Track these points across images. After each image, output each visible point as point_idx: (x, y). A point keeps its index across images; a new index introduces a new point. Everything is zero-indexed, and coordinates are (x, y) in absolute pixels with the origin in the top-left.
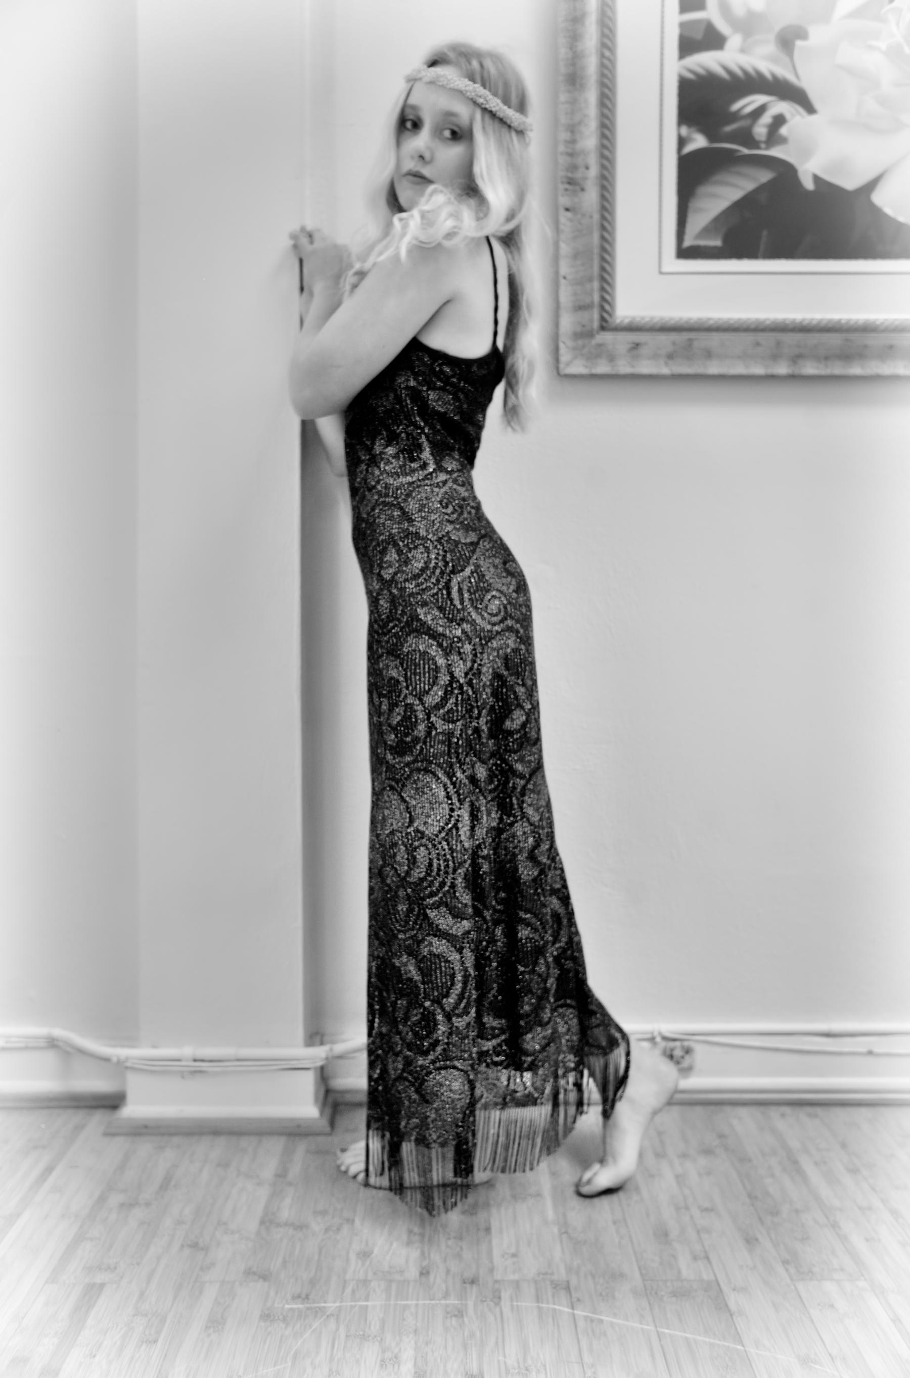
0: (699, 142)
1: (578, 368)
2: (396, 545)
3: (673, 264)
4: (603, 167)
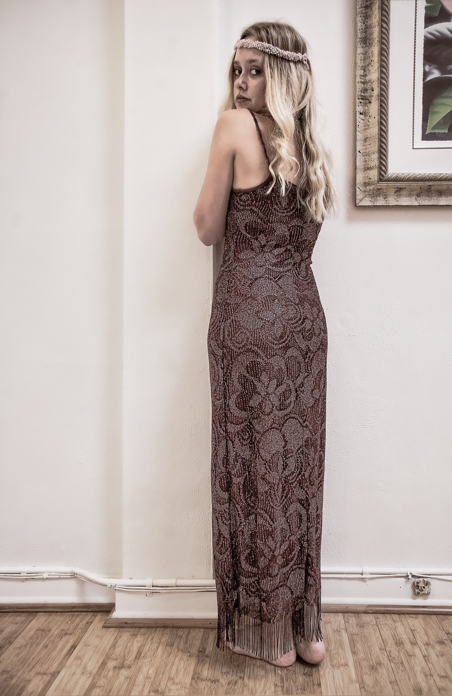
0: (436, 74)
1: (367, 202)
3: (420, 143)
4: (381, 89)
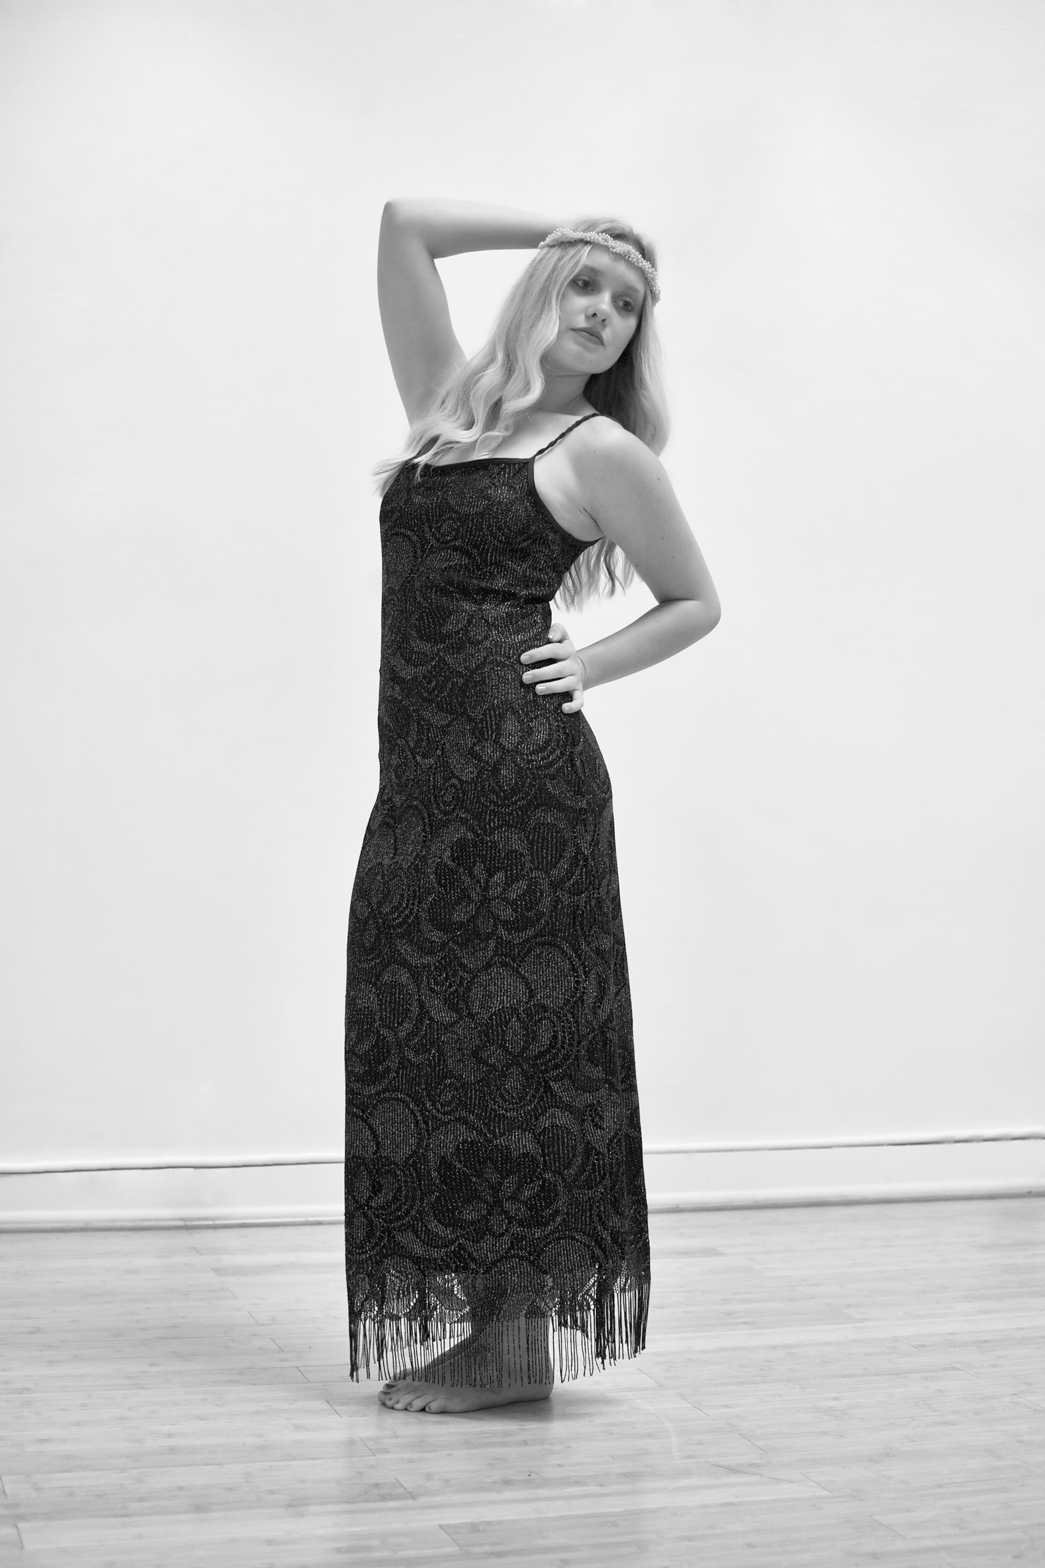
2: (515, 712)
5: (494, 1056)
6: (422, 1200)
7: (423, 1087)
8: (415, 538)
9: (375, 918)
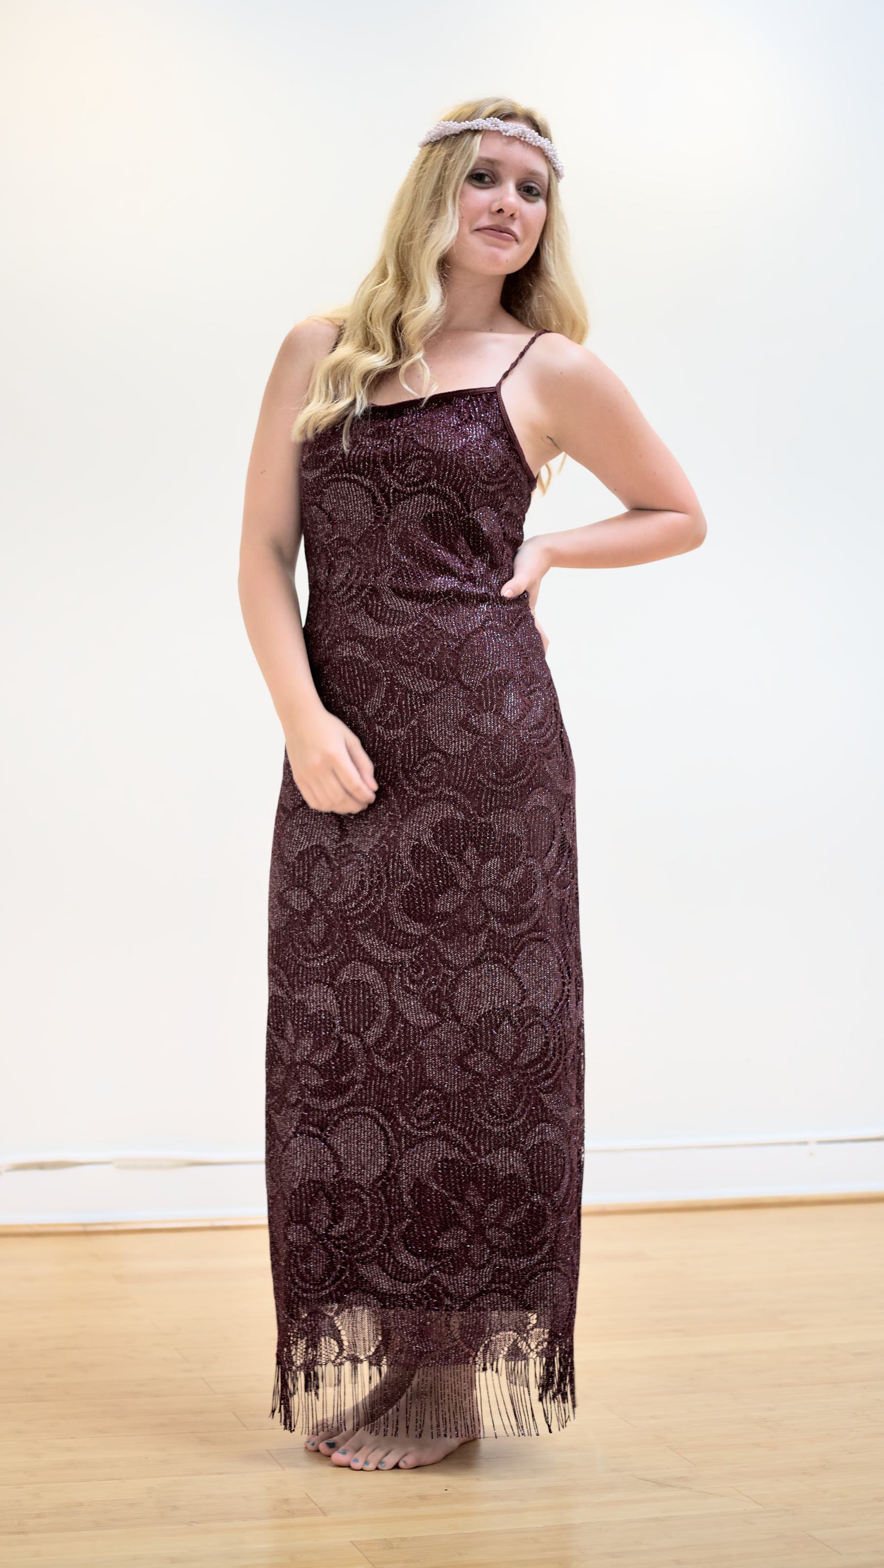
5: (481, 1063)
6: (390, 1228)
7: (396, 1099)
8: (367, 483)
9: (321, 908)
